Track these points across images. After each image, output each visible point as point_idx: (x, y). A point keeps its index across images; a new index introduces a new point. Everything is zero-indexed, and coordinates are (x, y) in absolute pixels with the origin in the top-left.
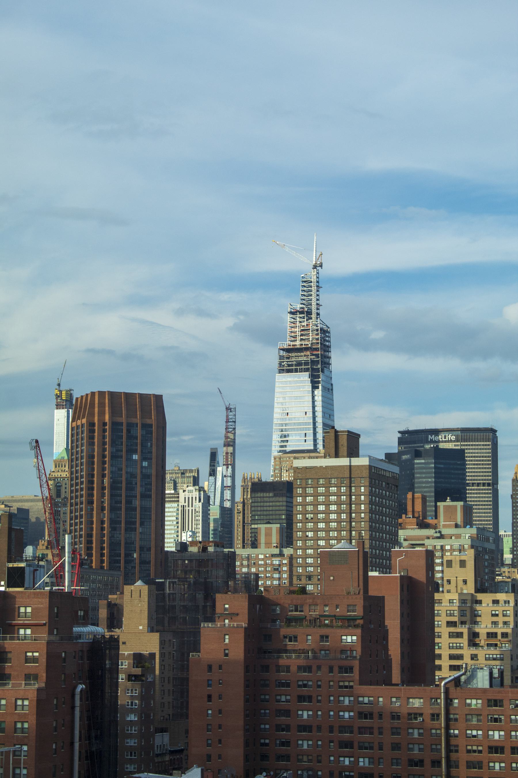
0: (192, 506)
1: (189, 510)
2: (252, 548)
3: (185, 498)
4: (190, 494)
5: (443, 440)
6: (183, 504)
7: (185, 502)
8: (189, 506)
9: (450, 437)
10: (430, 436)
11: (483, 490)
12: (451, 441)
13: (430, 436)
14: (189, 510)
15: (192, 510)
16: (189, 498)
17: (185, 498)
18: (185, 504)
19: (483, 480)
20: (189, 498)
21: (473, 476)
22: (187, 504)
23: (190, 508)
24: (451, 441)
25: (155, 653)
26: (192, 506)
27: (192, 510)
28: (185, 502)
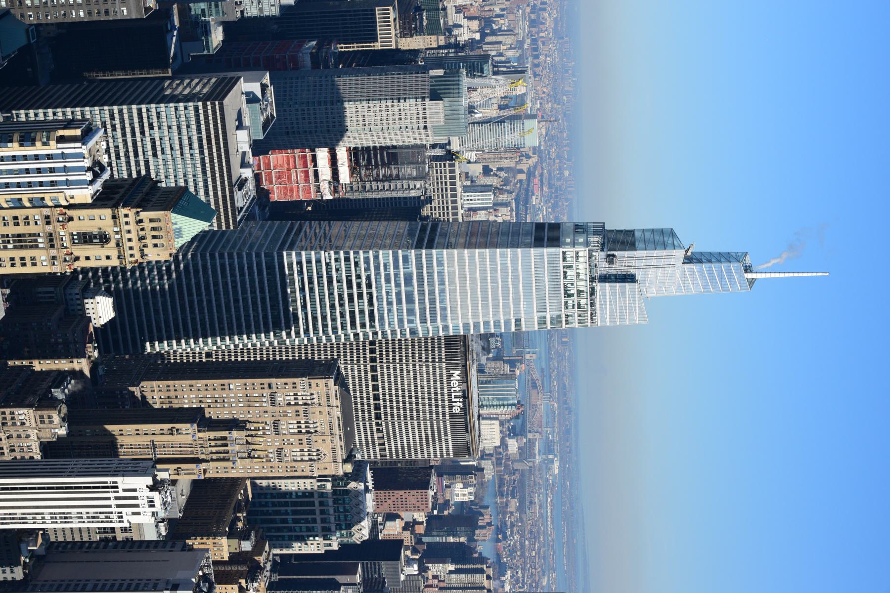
0: (118, 506)
1: (109, 499)
2: (632, 232)
3: (135, 490)
4: (145, 502)
5: (453, 394)
6: (121, 487)
7: (125, 490)
8: (117, 498)
9: (458, 404)
10: (458, 372)
11: (367, 387)
12: (451, 407)
13: (458, 372)
14: (109, 499)
15: (110, 506)
16: (136, 498)
17: (135, 490)
18: (120, 490)
19: (384, 394)
20: (136, 498)
21: (398, 403)
22: (121, 494)
23: (113, 502)
24: (451, 407)
25: (375, 40)
26: (118, 506)
27: (110, 506)
28: (125, 490)
